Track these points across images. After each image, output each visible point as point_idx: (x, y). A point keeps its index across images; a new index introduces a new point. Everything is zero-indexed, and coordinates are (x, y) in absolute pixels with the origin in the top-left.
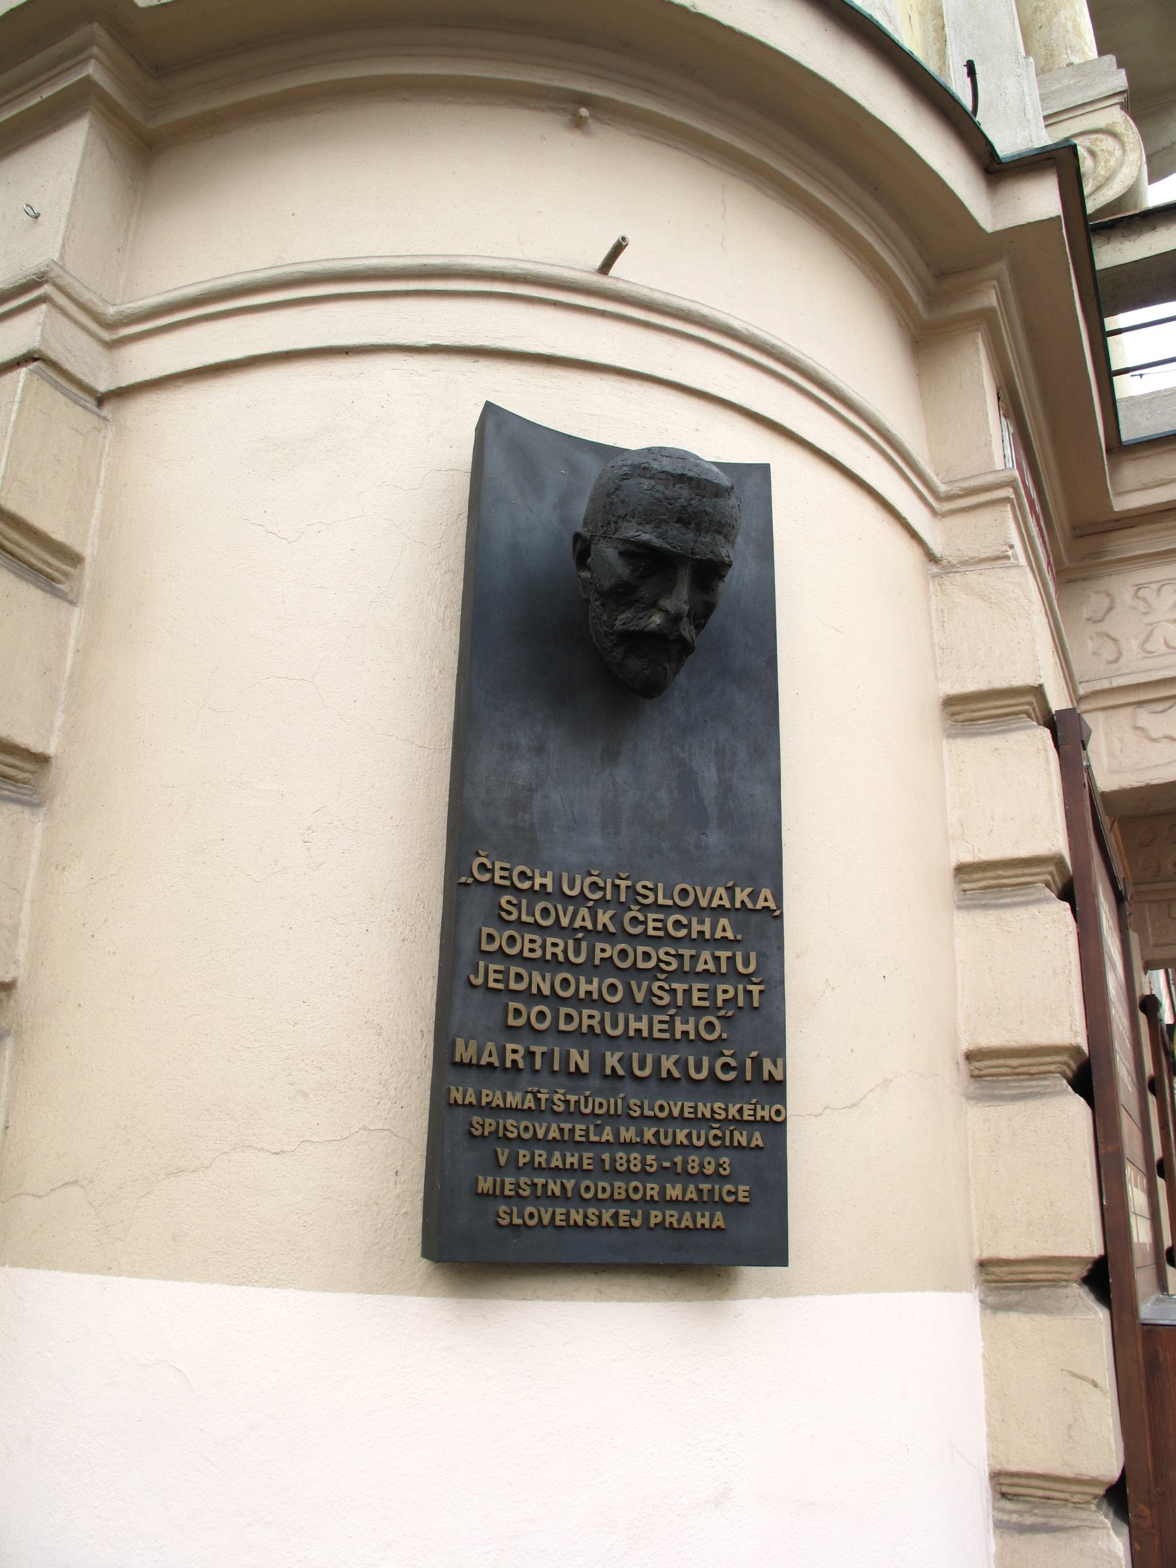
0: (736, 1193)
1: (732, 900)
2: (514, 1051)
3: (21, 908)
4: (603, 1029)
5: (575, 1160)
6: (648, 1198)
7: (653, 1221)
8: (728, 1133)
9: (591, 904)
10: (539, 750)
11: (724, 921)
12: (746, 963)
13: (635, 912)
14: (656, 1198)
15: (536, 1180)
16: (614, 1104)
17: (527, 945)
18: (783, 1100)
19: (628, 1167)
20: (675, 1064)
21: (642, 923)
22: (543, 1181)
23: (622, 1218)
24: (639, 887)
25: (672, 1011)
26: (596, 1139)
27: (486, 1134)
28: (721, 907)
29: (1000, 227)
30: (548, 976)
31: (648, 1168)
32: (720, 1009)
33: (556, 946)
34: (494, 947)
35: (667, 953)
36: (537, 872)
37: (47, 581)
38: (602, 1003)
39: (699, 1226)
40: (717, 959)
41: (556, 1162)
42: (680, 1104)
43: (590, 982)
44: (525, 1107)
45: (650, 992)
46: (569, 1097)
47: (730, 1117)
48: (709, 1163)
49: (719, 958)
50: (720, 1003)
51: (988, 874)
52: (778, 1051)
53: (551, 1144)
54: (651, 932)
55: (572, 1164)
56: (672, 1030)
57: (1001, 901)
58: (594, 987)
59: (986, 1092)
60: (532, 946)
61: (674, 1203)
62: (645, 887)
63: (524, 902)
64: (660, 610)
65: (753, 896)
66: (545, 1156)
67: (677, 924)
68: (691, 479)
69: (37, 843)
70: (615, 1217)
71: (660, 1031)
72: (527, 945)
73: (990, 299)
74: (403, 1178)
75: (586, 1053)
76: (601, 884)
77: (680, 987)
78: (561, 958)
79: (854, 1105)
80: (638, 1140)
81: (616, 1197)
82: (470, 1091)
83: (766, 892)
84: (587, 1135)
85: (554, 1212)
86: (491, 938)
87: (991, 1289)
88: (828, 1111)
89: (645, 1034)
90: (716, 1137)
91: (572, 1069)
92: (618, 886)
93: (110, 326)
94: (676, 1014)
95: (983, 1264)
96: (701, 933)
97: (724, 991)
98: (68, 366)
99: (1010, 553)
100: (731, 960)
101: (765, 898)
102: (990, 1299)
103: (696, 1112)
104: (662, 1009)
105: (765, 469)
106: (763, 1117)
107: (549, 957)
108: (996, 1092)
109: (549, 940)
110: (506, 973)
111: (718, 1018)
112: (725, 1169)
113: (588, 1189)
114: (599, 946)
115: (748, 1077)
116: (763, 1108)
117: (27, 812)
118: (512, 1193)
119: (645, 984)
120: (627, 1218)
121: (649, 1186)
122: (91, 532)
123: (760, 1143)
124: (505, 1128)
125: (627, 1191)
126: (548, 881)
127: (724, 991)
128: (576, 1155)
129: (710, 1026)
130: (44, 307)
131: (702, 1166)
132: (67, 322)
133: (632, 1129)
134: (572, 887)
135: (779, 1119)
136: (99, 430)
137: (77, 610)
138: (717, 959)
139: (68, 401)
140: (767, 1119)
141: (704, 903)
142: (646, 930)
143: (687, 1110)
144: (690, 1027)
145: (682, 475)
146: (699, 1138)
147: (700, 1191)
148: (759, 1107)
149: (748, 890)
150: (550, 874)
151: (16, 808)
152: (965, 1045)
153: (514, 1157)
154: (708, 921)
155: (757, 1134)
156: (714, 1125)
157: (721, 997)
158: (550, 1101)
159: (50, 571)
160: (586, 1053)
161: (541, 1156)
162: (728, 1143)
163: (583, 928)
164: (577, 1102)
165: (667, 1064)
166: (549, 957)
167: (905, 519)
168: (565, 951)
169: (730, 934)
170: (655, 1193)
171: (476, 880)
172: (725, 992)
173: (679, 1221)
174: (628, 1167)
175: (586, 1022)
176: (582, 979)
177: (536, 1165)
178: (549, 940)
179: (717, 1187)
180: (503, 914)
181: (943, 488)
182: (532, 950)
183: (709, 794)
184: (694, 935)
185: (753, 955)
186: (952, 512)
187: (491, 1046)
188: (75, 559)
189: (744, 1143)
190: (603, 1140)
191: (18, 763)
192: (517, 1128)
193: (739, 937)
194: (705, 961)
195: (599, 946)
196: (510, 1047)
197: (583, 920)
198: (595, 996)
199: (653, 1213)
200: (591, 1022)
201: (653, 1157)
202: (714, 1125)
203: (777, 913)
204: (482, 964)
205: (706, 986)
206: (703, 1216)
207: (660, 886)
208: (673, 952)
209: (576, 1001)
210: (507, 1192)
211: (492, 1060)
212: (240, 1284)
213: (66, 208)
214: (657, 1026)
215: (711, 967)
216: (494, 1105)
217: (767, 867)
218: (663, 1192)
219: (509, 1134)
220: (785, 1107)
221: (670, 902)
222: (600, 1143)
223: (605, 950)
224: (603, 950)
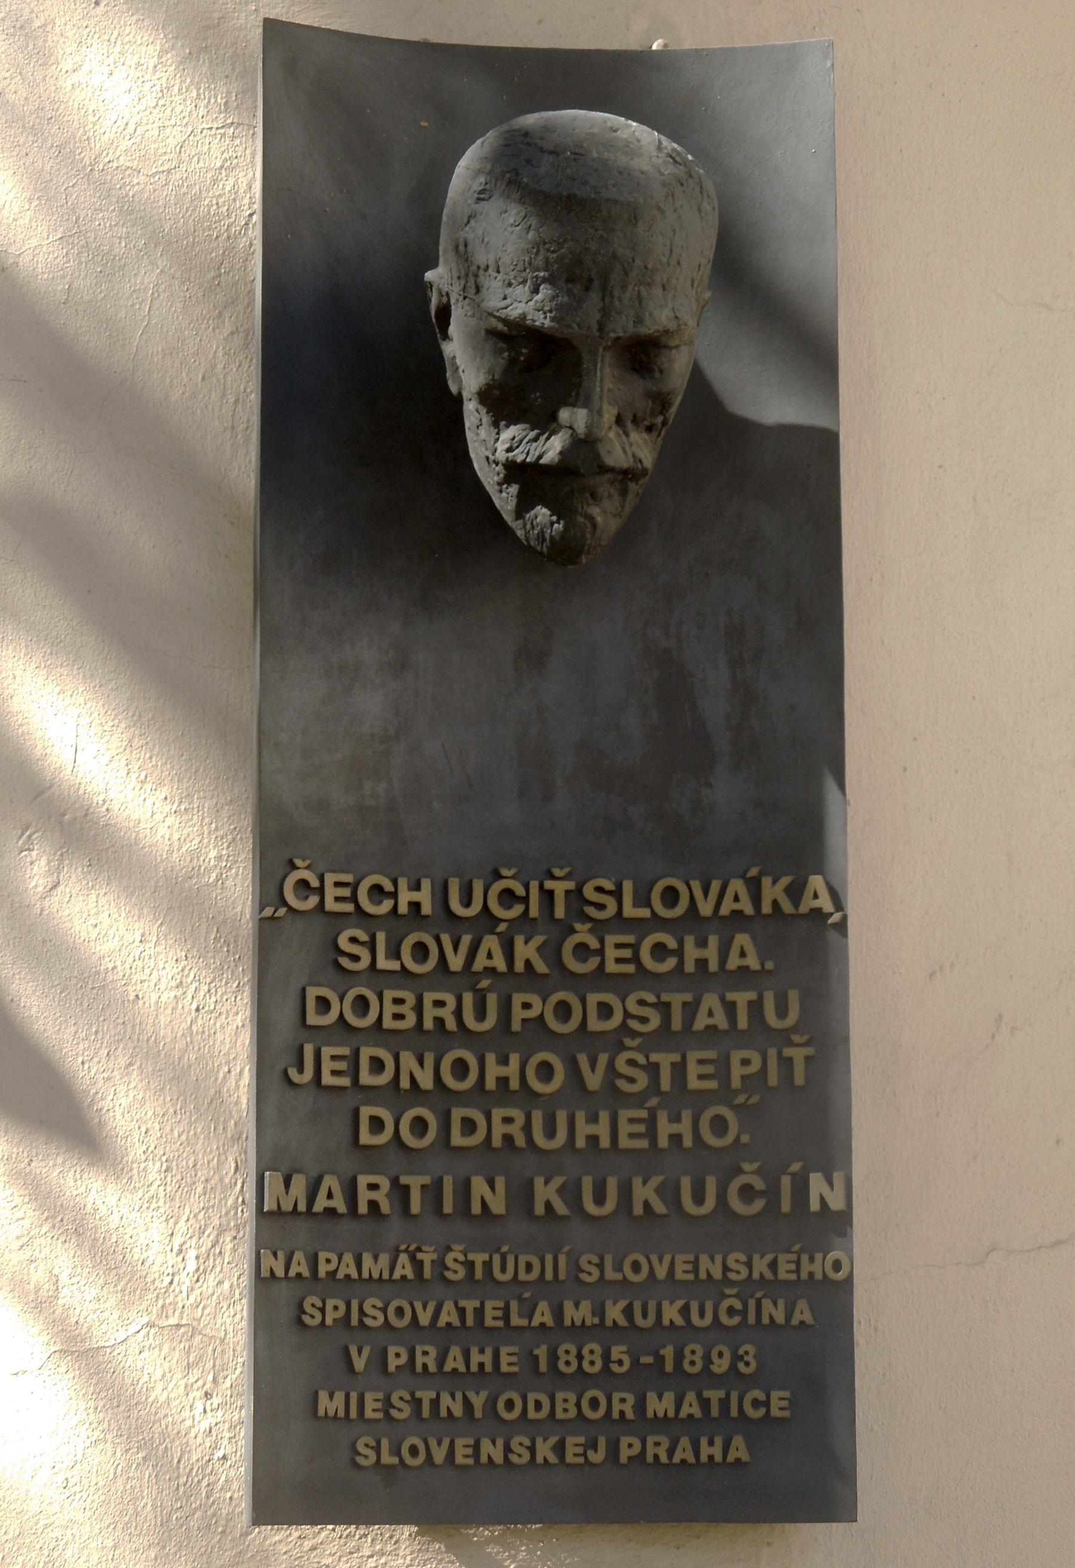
0: (767, 1404)
1: (756, 899)
5: (487, 1358)
6: (615, 1415)
8: (752, 1303)
11: (742, 939)
12: (782, 1012)
13: (583, 934)
14: (630, 1415)
17: (389, 1009)
20: (659, 1191)
25: (654, 1102)
26: (524, 1322)
28: (737, 914)
30: (429, 1059)
31: (615, 1368)
32: (736, 1093)
35: (642, 1002)
36: (403, 883)
40: (730, 1008)
41: (454, 1361)
42: (667, 1259)
43: (504, 1061)
46: (471, 1257)
47: (756, 1276)
48: (720, 1355)
49: (733, 1004)
55: (481, 1365)
58: (512, 1070)
60: (398, 1009)
61: (662, 1423)
62: (599, 889)
67: (660, 951)
70: (560, 1448)
72: (389, 1009)
74: (216, 1401)
75: (500, 1182)
76: (520, 891)
77: (665, 1060)
78: (451, 1025)
80: (596, 1321)
84: (506, 1318)
85: (452, 1444)
86: (324, 1004)
89: (605, 1142)
96: (702, 963)
100: (756, 1008)
103: (696, 1271)
106: (811, 1275)
107: (428, 1024)
109: (429, 998)
112: (747, 1364)
114: (518, 999)
116: (812, 1259)
119: (603, 1059)
120: (580, 1450)
123: (808, 1318)
124: (362, 1313)
125: (578, 1405)
126: (425, 897)
128: (489, 1351)
129: (720, 1125)
131: (707, 1360)
133: (586, 1306)
134: (467, 903)
135: (841, 1275)
138: (730, 1008)
140: (819, 1276)
142: (602, 963)
144: (685, 1127)
145: (570, 197)
146: (702, 1315)
148: (805, 1258)
149: (785, 881)
154: (713, 941)
155: (802, 1305)
156: (728, 1291)
157: (737, 1072)
158: (440, 1264)
160: (500, 1182)
162: (751, 1319)
163: (491, 971)
164: (488, 1265)
165: (644, 1192)
166: (428, 1024)
168: (458, 1013)
169: (753, 962)
171: (291, 909)
172: (745, 1062)
173: (671, 1452)
175: (499, 1130)
176: (491, 1058)
177: (419, 1368)
179: (734, 1396)
183: (715, 708)
185: (794, 997)
187: (330, 1182)
189: (780, 1318)
192: (384, 1310)
193: (770, 965)
194: (711, 1012)
197: (490, 956)
199: (624, 1441)
201: (624, 1348)
202: (728, 1291)
203: (836, 917)
204: (309, 1050)
205: (712, 1054)
206: (711, 1443)
207: (628, 886)
208: (651, 998)
214: (624, 1129)
215: (720, 1020)
216: (340, 1275)
218: (641, 1405)
219: (368, 1321)
221: (645, 913)
223: (529, 1006)
224: (526, 1006)
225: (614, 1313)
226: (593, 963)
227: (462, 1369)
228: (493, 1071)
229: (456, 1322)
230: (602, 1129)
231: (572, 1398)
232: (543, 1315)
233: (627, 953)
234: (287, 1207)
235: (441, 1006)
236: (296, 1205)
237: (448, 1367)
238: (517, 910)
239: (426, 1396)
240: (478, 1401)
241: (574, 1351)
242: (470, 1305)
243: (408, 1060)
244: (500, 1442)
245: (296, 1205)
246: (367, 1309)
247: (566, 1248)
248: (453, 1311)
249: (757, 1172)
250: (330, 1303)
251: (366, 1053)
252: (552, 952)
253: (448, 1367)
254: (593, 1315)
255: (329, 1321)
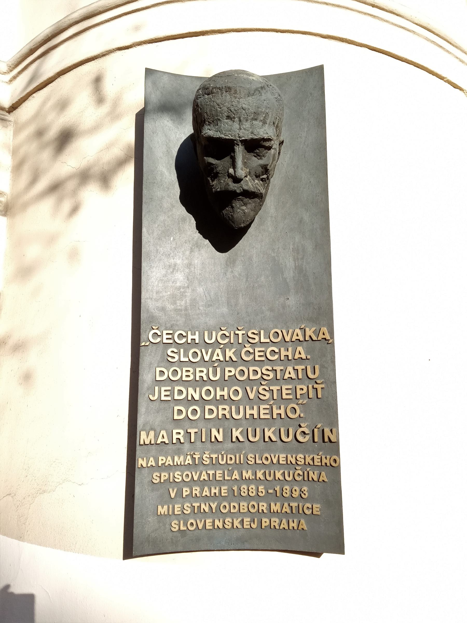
5: (217, 491)
8: (306, 473)
11: (300, 349)
17: (185, 374)
20: (273, 432)
26: (229, 478)
30: (198, 389)
31: (260, 494)
36: (189, 333)
41: (206, 492)
42: (277, 456)
58: (225, 393)
60: (188, 374)
77: (275, 388)
78: (205, 378)
109: (198, 369)
114: (227, 369)
126: (196, 337)
128: (217, 488)
158: (201, 459)
160: (221, 430)
164: (217, 458)
168: (208, 375)
169: (303, 356)
176: (218, 389)
185: (317, 367)
192: (182, 476)
193: (309, 357)
207: (262, 332)
208: (270, 368)
214: (262, 412)
215: (293, 375)
216: (166, 464)
219: (176, 480)
223: (230, 371)
224: (230, 371)
225: (260, 475)
226: (251, 357)
227: (208, 495)
228: (219, 393)
229: (206, 479)
230: (255, 412)
231: (246, 504)
232: (236, 475)
233: (170, 336)
234: (147, 442)
235: (202, 373)
236: (151, 441)
237: (204, 494)
238: (227, 340)
239: (196, 505)
240: (214, 506)
241: (246, 488)
242: (211, 472)
243: (191, 390)
244: (221, 521)
245: (151, 441)
246: (176, 476)
247: (243, 452)
248: (205, 475)
249: (306, 427)
250: (163, 474)
251: (177, 388)
252: (238, 353)
253: (204, 494)
254: (252, 475)
255: (162, 481)
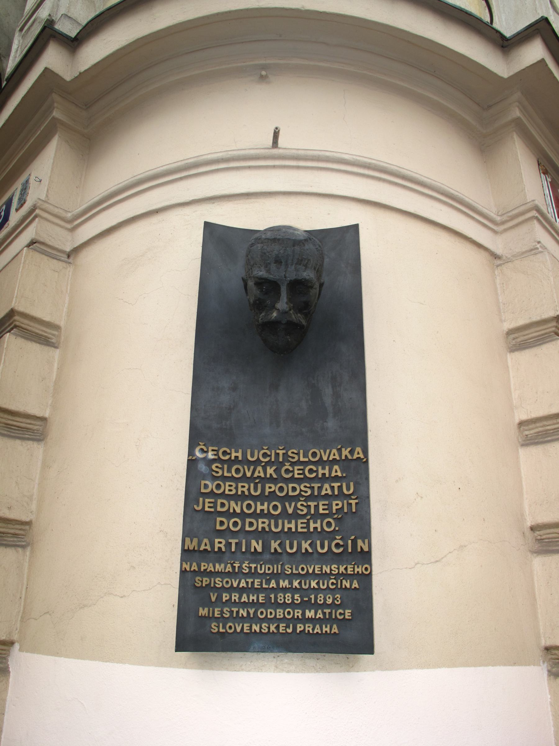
0: (344, 614)
1: (340, 455)
2: (219, 543)
3: (34, 488)
4: (270, 529)
5: (255, 598)
6: (296, 617)
7: (299, 630)
8: (339, 581)
9: (263, 464)
10: (234, 388)
11: (336, 467)
12: (348, 489)
13: (287, 466)
14: (300, 617)
15: (232, 609)
16: (277, 568)
17: (227, 488)
18: (369, 562)
19: (285, 601)
21: (315, 471)
22: (237, 609)
23: (281, 629)
24: (290, 453)
25: (309, 517)
26: (267, 586)
27: (204, 585)
29: (511, 73)
30: (239, 503)
31: (296, 601)
32: (335, 514)
33: (243, 488)
34: (208, 490)
35: (305, 487)
37: (45, 341)
38: (269, 515)
39: (324, 632)
40: (332, 488)
41: (244, 599)
42: (313, 567)
44: (227, 571)
45: (296, 508)
47: (340, 572)
48: (329, 598)
50: (334, 511)
51: (538, 425)
52: (366, 534)
53: (241, 591)
54: (296, 476)
56: (308, 527)
57: (546, 439)
58: (265, 507)
59: (545, 548)
61: (310, 620)
62: (293, 453)
63: (226, 466)
64: (276, 309)
65: (352, 452)
66: (238, 596)
67: (311, 471)
68: (279, 240)
69: (41, 457)
71: (302, 528)
73: (517, 113)
75: (260, 542)
76: (269, 453)
77: (312, 504)
78: (247, 493)
79: (437, 561)
80: (290, 586)
81: (278, 617)
82: (194, 564)
83: (358, 449)
84: (261, 585)
85: (243, 626)
87: (555, 664)
88: (418, 566)
90: (333, 584)
91: (253, 550)
92: (278, 454)
93: (70, 221)
94: (310, 518)
95: (547, 649)
96: (324, 474)
97: (336, 505)
98: (50, 243)
99: (538, 246)
100: (340, 488)
101: (358, 453)
102: (554, 670)
103: (322, 570)
104: (304, 516)
105: (355, 228)
106: (358, 572)
107: (239, 493)
108: (550, 548)
110: (215, 503)
111: (334, 519)
112: (338, 601)
113: (262, 613)
115: (350, 550)
117: (35, 445)
118: (219, 616)
119: (293, 504)
120: (284, 628)
121: (296, 611)
122: (64, 314)
124: (215, 582)
125: (284, 613)
127: (336, 505)
128: (256, 596)
129: (329, 524)
130: (37, 220)
132: (49, 224)
136: (66, 268)
137: (58, 350)
138: (332, 488)
139: (49, 258)
140: (360, 572)
141: (325, 458)
142: (293, 475)
143: (316, 569)
144: (318, 525)
147: (324, 614)
148: (356, 566)
150: (240, 451)
151: (30, 442)
152: (529, 523)
153: (219, 598)
154: (327, 468)
156: (332, 577)
157: (335, 508)
159: (46, 335)
161: (235, 597)
162: (339, 586)
163: (259, 477)
167: (471, 238)
168: (249, 490)
169: (339, 474)
170: (300, 615)
172: (337, 505)
173: (313, 629)
174: (285, 601)
176: (259, 503)
178: (240, 485)
179: (334, 611)
180: (214, 474)
181: (498, 219)
182: (230, 490)
184: (320, 476)
185: (352, 484)
186: (505, 230)
188: (57, 327)
189: (348, 586)
190: (271, 587)
191: (32, 422)
193: (344, 475)
194: (326, 489)
195: (267, 485)
196: (217, 540)
198: (266, 512)
199: (299, 625)
200: (263, 525)
202: (332, 577)
203: (365, 460)
204: (201, 499)
205: (327, 502)
206: (326, 627)
207: (301, 451)
208: (308, 485)
209: (255, 515)
210: (216, 615)
211: (206, 548)
212: (106, 662)
213: (49, 175)
216: (208, 570)
217: (358, 435)
218: (303, 614)
220: (371, 565)
222: (269, 588)
223: (270, 488)
